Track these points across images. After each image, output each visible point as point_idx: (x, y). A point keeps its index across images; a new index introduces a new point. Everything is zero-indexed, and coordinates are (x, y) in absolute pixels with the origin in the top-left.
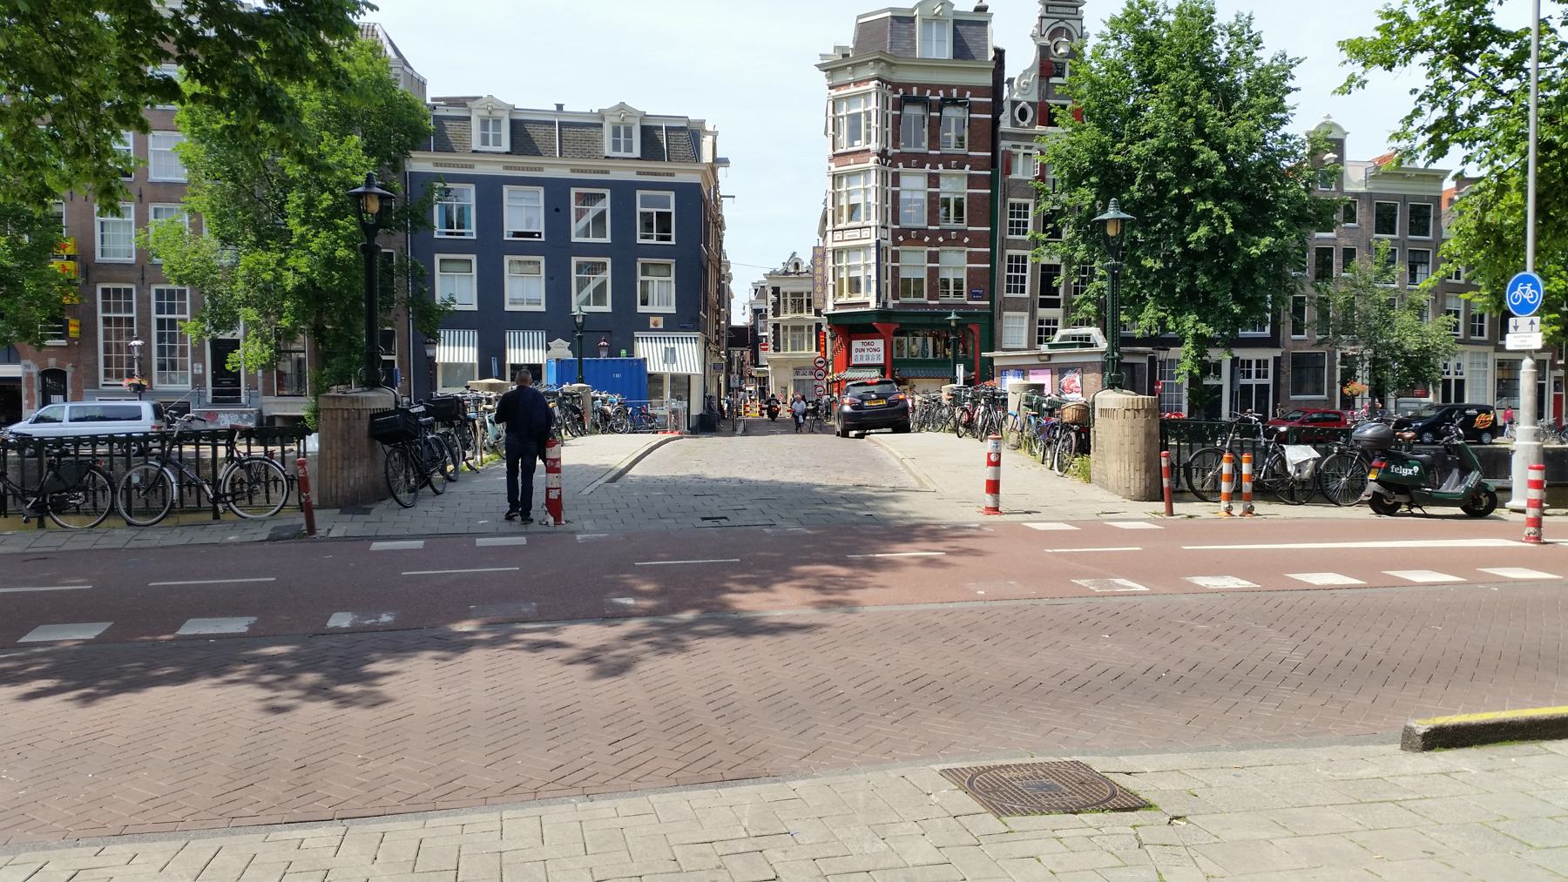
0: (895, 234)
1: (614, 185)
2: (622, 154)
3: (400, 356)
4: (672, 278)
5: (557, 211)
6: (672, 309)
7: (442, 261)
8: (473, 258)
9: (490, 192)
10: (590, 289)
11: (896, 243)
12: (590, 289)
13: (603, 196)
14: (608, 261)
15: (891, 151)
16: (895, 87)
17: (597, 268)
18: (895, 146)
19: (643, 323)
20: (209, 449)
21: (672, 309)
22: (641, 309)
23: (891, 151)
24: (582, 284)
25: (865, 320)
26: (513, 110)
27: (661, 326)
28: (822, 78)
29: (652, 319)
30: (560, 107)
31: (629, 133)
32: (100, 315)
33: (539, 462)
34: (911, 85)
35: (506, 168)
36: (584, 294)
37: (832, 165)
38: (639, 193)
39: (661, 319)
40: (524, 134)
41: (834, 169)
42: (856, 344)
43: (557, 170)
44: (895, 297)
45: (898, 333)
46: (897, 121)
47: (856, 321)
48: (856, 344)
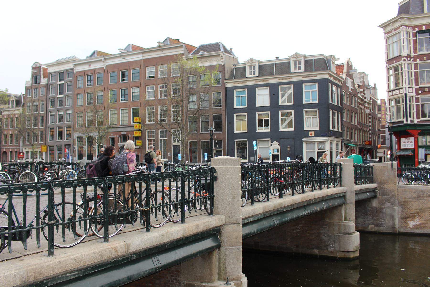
0: (417, 90)
1: (248, 87)
2: (252, 76)
3: (224, 150)
4: (318, 116)
5: (274, 96)
6: (318, 128)
7: (237, 116)
8: (246, 114)
9: (298, 87)
10: (286, 123)
11: (417, 94)
12: (286, 123)
13: (291, 87)
14: (293, 111)
15: (413, 54)
16: (414, 28)
17: (290, 114)
18: (415, 52)
19: (306, 134)
20: (175, 183)
21: (318, 128)
22: (305, 129)
23: (413, 54)
24: (284, 120)
25: (402, 129)
26: (305, 57)
27: (313, 135)
28: (382, 30)
29: (310, 133)
30: (277, 58)
31: (300, 63)
32: (147, 139)
33: (295, 191)
34: (422, 26)
35: (303, 77)
36: (284, 125)
37: (387, 65)
38: (280, 87)
39: (313, 133)
40: (265, 69)
41: (388, 66)
42: (403, 140)
43: (273, 80)
44: (418, 118)
45: (420, 134)
46: (415, 42)
47: (400, 129)
48: (403, 140)
